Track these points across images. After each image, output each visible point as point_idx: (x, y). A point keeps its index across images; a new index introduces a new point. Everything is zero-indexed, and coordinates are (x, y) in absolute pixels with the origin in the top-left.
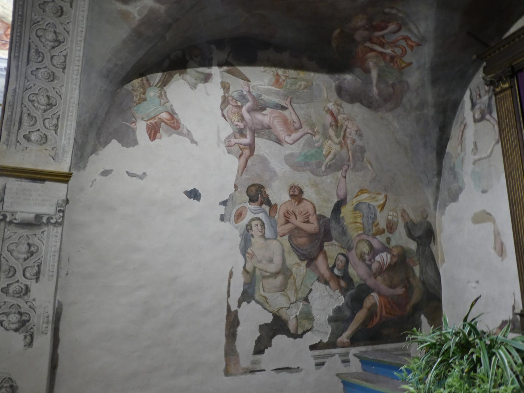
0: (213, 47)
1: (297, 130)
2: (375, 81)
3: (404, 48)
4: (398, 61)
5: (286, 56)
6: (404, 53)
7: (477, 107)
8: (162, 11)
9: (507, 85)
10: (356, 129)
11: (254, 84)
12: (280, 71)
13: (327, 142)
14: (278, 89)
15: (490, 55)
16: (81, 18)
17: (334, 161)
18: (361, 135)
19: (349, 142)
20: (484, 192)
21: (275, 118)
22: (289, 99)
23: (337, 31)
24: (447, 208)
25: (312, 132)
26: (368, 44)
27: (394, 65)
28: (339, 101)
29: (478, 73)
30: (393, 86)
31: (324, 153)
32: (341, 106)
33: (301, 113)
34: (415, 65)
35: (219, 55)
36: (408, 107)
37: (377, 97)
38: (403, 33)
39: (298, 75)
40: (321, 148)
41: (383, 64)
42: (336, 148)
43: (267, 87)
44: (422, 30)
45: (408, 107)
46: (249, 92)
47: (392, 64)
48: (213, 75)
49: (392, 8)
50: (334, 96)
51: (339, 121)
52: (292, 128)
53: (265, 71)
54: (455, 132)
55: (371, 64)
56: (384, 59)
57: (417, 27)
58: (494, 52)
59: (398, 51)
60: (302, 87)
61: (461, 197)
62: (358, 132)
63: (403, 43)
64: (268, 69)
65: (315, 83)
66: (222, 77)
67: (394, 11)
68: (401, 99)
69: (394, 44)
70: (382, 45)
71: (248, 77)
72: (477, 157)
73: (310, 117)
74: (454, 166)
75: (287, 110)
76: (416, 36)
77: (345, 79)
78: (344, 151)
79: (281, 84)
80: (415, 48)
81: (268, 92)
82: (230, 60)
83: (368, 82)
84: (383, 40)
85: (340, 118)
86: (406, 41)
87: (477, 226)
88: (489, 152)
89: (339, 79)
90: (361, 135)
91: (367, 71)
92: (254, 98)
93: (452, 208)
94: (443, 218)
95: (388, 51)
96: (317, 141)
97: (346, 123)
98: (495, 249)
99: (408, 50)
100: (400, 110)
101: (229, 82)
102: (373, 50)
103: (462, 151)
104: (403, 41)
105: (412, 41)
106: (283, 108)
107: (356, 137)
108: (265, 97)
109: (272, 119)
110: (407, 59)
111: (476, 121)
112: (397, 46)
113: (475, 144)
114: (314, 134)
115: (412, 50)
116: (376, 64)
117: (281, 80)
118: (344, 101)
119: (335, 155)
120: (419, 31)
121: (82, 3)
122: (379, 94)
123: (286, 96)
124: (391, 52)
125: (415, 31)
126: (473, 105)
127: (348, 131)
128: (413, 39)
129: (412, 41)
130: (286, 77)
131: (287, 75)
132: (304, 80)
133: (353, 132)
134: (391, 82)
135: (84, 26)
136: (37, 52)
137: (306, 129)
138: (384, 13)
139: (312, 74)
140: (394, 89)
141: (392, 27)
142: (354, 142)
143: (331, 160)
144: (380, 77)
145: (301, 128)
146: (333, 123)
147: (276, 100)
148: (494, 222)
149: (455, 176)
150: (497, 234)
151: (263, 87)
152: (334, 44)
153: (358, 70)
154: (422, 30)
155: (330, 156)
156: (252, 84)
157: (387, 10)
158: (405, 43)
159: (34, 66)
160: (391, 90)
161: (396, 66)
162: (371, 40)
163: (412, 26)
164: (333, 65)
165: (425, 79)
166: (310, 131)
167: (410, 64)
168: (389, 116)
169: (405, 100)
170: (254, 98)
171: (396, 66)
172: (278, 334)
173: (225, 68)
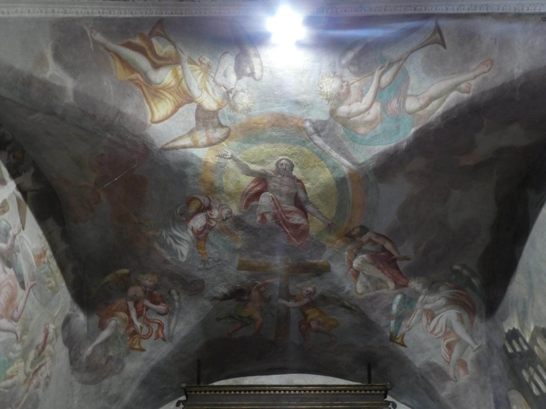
0: (32, 170)
1: (12, 319)
2: (98, 341)
3: (152, 333)
4: (136, 339)
5: (63, 246)
6: (147, 337)
8: (66, 101)
10: (49, 373)
11: (25, 236)
12: (49, 253)
13: (21, 362)
14: (35, 264)
15: (196, 392)
16: (19, 10)
17: (7, 391)
18: (47, 384)
19: (34, 382)
21: (9, 284)
22: (33, 283)
23: (126, 271)
25: (19, 336)
26: (131, 304)
27: (129, 340)
28: (59, 331)
29: (170, 404)
30: (110, 358)
31: (8, 372)
32: (57, 337)
33: (29, 305)
34: (144, 354)
35: (27, 179)
36: (102, 391)
37: (84, 357)
39: (56, 272)
40: (11, 361)
41: (122, 331)
42: (21, 377)
43: (30, 251)
44: (177, 329)
45: (102, 391)
46: (15, 236)
47: (128, 338)
48: (6, 187)
49: (178, 294)
50: (60, 323)
51: (45, 351)
52: (11, 312)
53: (41, 238)
55: (112, 323)
56: (127, 328)
57: (176, 324)
58: (201, 392)
59: (145, 331)
60: (50, 285)
62: (48, 379)
63: (155, 327)
64: (44, 238)
65: (59, 293)
66: (10, 197)
67: (176, 297)
68: (103, 378)
69: (148, 322)
70: (139, 315)
71: (26, 225)
73: (31, 320)
75: (23, 291)
76: (169, 330)
77: (78, 316)
78: (23, 388)
79: (40, 262)
80: (160, 339)
81: (26, 257)
82: (29, 195)
83: (91, 336)
84: (144, 312)
85: (48, 347)
86: (159, 328)
89: (74, 311)
90: (47, 384)
91: (102, 326)
92: (12, 246)
96: (14, 352)
97: (48, 358)
99: (153, 336)
100: (92, 389)
101: (11, 208)
102: (128, 312)
104: (157, 325)
105: (162, 332)
106: (22, 285)
107: (42, 383)
108: (20, 256)
109: (6, 283)
110: (145, 344)
112: (148, 326)
114: (19, 340)
115: (155, 339)
116: (117, 326)
117: (43, 260)
118: (63, 336)
119: (14, 385)
120: (174, 328)
121: (37, 9)
122: (89, 358)
123: (33, 277)
124: (139, 327)
125: (172, 326)
127: (43, 368)
128: (165, 331)
129: (162, 332)
130: (48, 262)
131: (50, 261)
132: (55, 281)
133: (45, 375)
134: (111, 354)
135: (11, 15)
137: (18, 327)
138: (169, 293)
139: (64, 284)
140: (106, 363)
141: (162, 308)
142: (38, 386)
143: (6, 388)
145: (16, 321)
146: (40, 347)
147: (25, 271)
151: (28, 247)
152: (108, 278)
153: (96, 319)
154: (177, 329)
155: (9, 382)
156: (23, 233)
157: (173, 292)
158: (157, 329)
160: (103, 361)
161: (131, 341)
162: (136, 303)
163: (174, 320)
165: (141, 374)
166: (19, 333)
167: (143, 350)
168: (78, 387)
169: (106, 382)
170: (12, 246)
171: (131, 341)
172: (524, 397)
173: (19, 194)
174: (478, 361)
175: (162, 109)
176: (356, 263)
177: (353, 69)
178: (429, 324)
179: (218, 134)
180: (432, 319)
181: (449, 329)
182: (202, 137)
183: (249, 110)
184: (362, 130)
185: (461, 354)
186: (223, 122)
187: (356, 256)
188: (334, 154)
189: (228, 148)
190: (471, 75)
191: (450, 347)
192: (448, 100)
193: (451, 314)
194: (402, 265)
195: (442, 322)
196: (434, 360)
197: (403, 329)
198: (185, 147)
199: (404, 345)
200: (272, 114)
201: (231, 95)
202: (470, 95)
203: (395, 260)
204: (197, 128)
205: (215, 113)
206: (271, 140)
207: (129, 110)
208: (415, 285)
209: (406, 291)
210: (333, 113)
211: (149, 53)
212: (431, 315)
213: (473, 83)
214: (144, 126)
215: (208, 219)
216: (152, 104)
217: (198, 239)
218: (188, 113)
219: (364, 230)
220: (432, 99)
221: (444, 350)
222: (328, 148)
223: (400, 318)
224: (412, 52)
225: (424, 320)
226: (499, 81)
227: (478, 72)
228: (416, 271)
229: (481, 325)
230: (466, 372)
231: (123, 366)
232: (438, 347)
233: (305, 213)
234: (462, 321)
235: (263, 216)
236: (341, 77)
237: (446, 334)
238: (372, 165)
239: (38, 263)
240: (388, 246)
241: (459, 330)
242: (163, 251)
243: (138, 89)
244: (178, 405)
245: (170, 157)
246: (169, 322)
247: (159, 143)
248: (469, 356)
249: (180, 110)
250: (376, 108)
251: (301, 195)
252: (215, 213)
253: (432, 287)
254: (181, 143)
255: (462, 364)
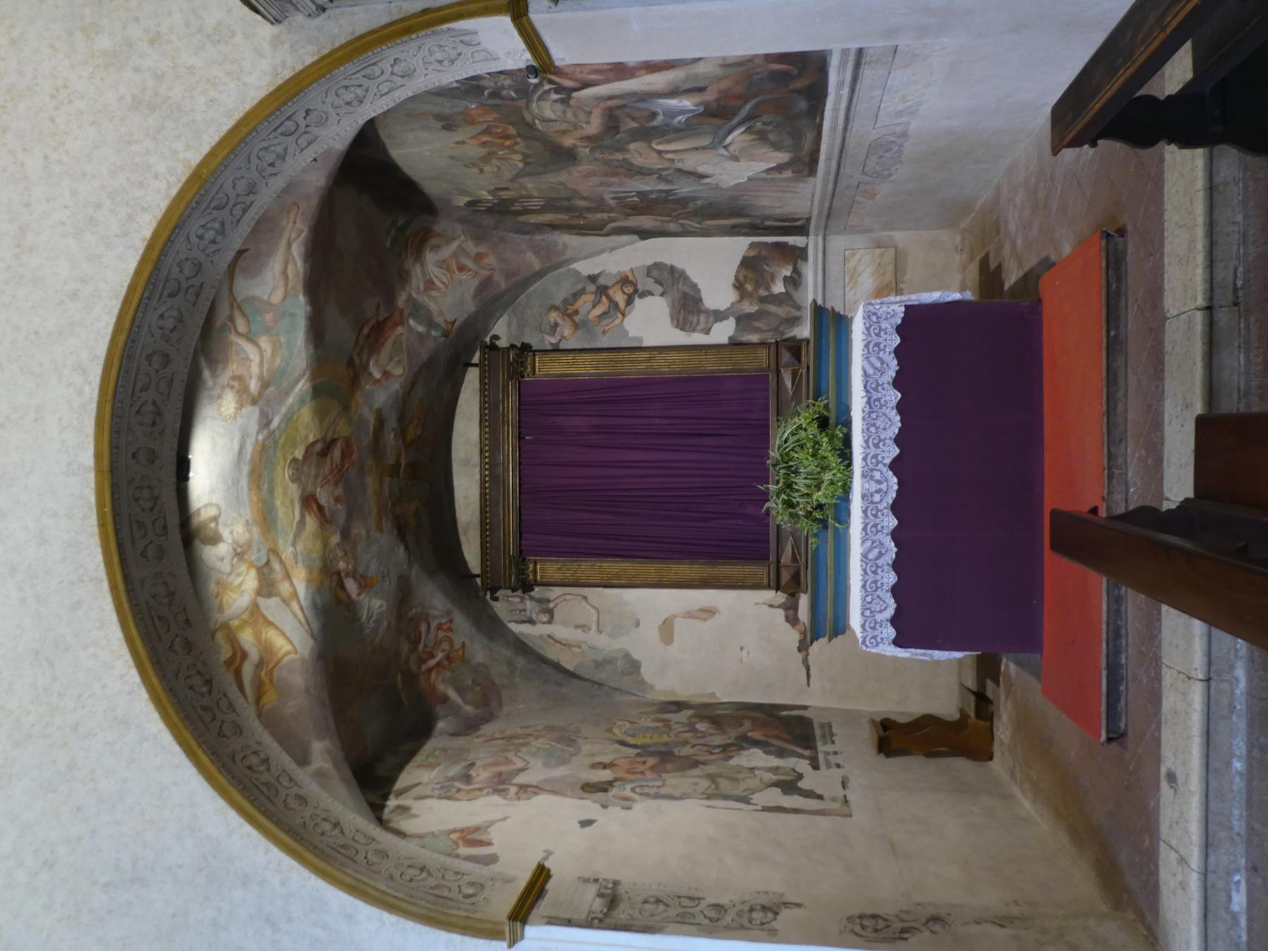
6: (451, 641)
7: (534, 617)
9: (531, 566)
20: (637, 624)
24: (646, 679)
34: (467, 643)
37: (479, 711)
38: (434, 624)
41: (448, 674)
44: (440, 607)
54: (552, 653)
55: (441, 687)
59: (445, 646)
61: (636, 656)
63: (441, 634)
69: (438, 643)
70: (432, 656)
72: (594, 627)
74: (595, 661)
83: (456, 711)
87: (676, 638)
88: (593, 611)
91: (445, 699)
93: (647, 673)
94: (658, 687)
95: (440, 656)
98: (706, 620)
102: (430, 670)
103: (579, 647)
110: (457, 645)
111: (550, 622)
112: (440, 643)
113: (577, 627)
116: (443, 681)
122: (477, 707)
126: (531, 621)
128: (444, 621)
136: (343, 846)
140: (479, 685)
141: (423, 627)
144: (460, 691)
148: (676, 616)
149: (609, 661)
150: (689, 615)
153: (440, 710)
154: (440, 607)
159: (360, 857)
160: (478, 689)
164: (421, 730)
168: (506, 709)
169: (497, 680)
174: (477, 239)
175: (280, 644)
176: (377, 375)
177: (219, 371)
178: (438, 289)
179: (276, 566)
180: (433, 283)
181: (443, 264)
182: (284, 588)
183: (247, 522)
184: (278, 361)
185: (468, 256)
186: (264, 560)
187: (370, 374)
188: (290, 400)
189: (287, 552)
190: (290, 225)
191: (462, 268)
192: (295, 254)
193: (430, 257)
194: (383, 315)
195: (437, 271)
196: (472, 290)
197: (440, 320)
198: (302, 609)
199: (453, 323)
200: (250, 489)
201: (239, 550)
202: (306, 230)
203: (378, 323)
204: (278, 594)
205: (260, 570)
206: (271, 491)
207: (298, 680)
208: (401, 301)
209: (406, 313)
210: (254, 402)
211: (237, 664)
212: (430, 284)
213: (298, 225)
214: (303, 661)
215: (347, 575)
216: (280, 654)
217: (366, 586)
218: (270, 607)
219: (351, 363)
220: (285, 273)
221: (464, 276)
222: (284, 409)
223: (431, 324)
224: (231, 290)
225: (434, 293)
226: (315, 201)
227: (292, 220)
228: (390, 299)
229: (442, 225)
230: (486, 255)
231: (480, 665)
232: (461, 282)
233: (334, 441)
234: (436, 248)
235: (337, 500)
236: (223, 387)
237: (448, 269)
238: (311, 350)
239: (439, 765)
240: (366, 331)
241: (446, 252)
242: (380, 631)
243: (276, 673)
244: (496, 599)
245: (316, 626)
246: (436, 617)
247: (310, 643)
248: (472, 247)
249: (271, 619)
250: (264, 342)
251: (318, 447)
252: (342, 565)
253: (404, 277)
254: (299, 614)
255: (478, 257)
